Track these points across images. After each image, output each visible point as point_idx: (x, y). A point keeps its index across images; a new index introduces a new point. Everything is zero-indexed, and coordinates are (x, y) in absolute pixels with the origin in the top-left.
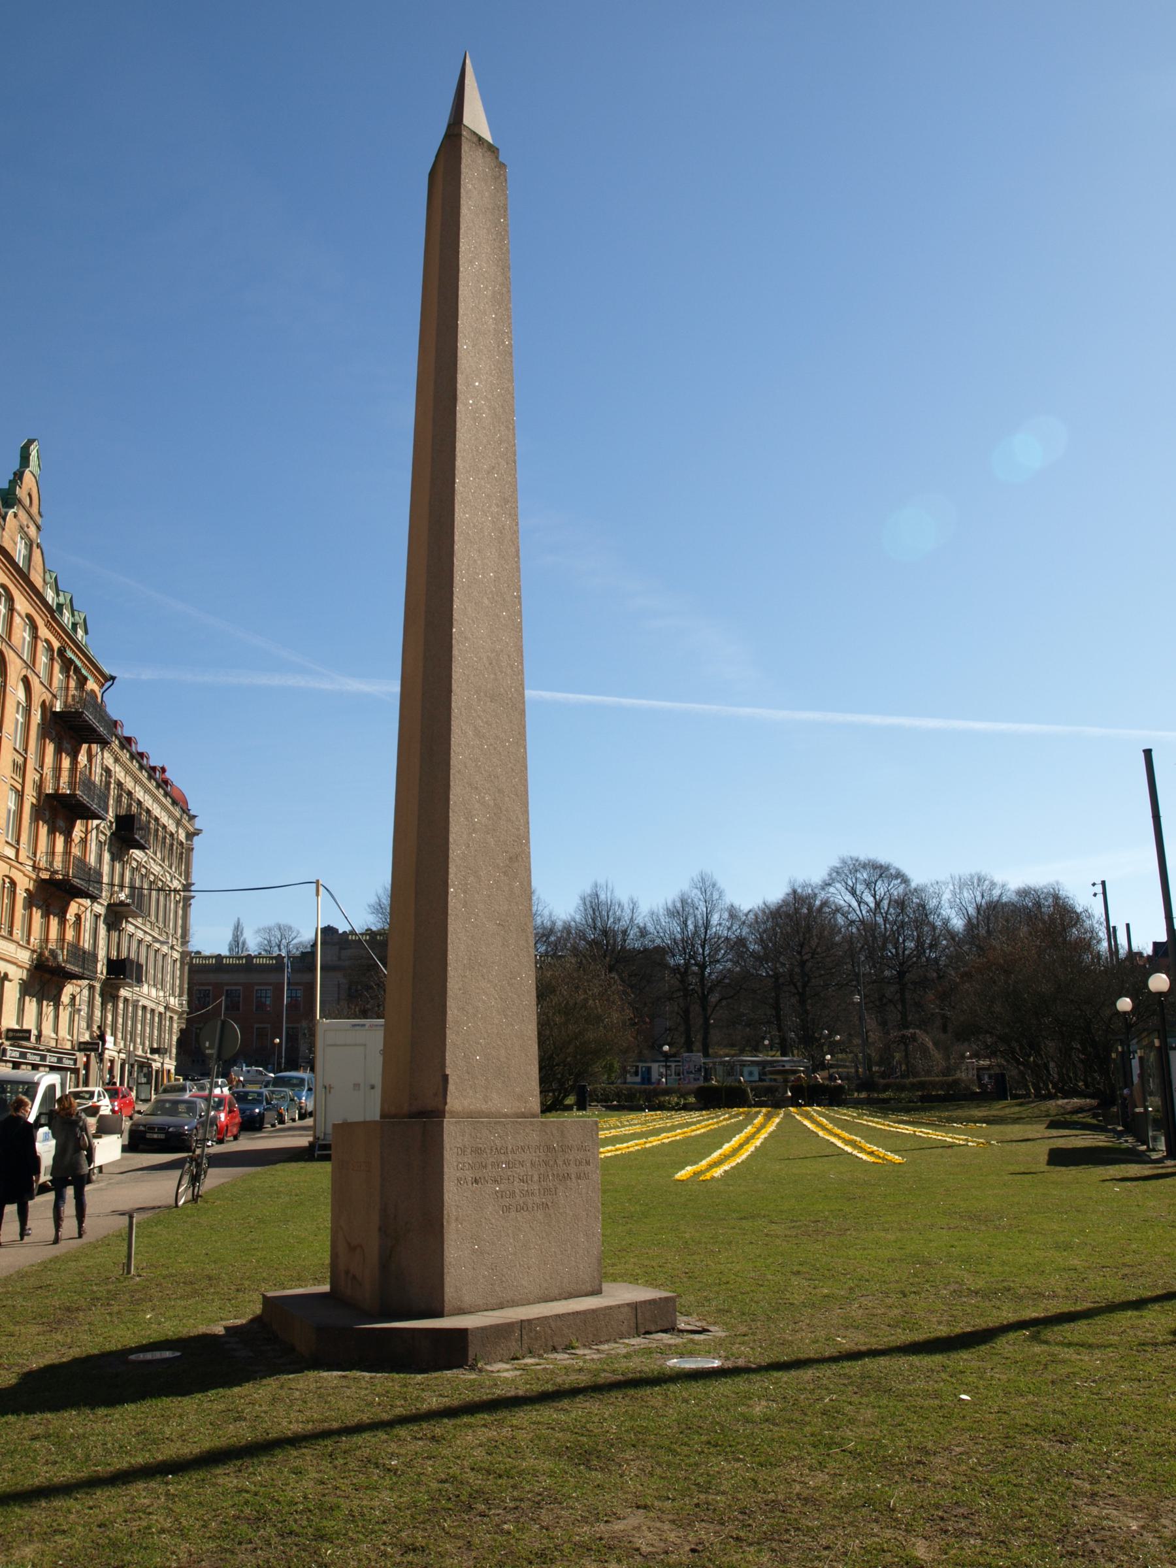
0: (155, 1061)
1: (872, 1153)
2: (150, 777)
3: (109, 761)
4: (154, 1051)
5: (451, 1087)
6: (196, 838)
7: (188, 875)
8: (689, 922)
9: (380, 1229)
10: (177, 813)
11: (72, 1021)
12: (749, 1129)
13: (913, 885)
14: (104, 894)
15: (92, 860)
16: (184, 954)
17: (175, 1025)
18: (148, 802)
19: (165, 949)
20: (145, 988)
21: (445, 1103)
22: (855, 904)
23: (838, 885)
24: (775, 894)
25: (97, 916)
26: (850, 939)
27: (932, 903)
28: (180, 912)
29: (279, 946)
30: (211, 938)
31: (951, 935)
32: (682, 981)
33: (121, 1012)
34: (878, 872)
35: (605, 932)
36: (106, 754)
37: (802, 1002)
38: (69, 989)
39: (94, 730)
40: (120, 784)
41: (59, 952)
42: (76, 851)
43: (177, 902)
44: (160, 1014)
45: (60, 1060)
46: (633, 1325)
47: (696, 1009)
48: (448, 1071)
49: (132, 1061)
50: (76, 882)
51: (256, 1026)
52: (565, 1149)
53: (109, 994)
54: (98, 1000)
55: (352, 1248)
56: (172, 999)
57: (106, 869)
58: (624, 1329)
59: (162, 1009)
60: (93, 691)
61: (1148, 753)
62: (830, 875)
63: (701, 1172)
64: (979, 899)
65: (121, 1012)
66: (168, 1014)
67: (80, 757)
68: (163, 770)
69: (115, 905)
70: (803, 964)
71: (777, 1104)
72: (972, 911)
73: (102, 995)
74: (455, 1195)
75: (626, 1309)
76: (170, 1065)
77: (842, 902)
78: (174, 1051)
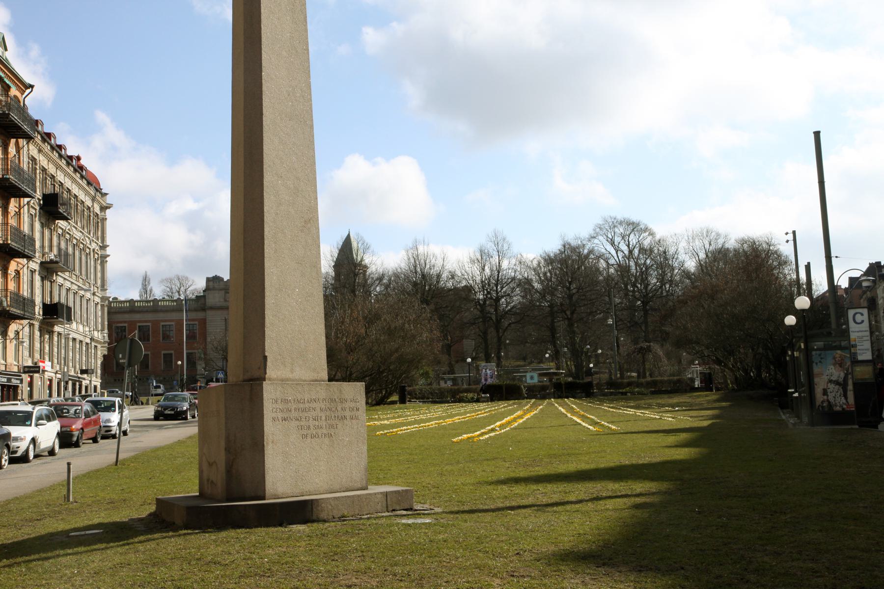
0: (84, 379)
1: (595, 424)
2: (68, 164)
3: (34, 152)
4: (83, 372)
5: (269, 364)
6: (108, 211)
7: (103, 239)
8: (486, 268)
9: (226, 449)
10: (92, 192)
11: (17, 350)
12: (519, 413)
13: (658, 237)
14: (37, 255)
15: (26, 229)
16: (103, 299)
17: (99, 353)
18: (68, 183)
19: (88, 295)
20: (74, 325)
21: (266, 373)
22: (613, 252)
23: (601, 238)
24: (553, 247)
25: (33, 272)
26: (609, 277)
27: (672, 250)
28: (99, 267)
29: (179, 292)
30: (126, 291)
31: (686, 274)
32: (482, 311)
33: (55, 343)
34: (631, 227)
35: (424, 276)
36: (31, 147)
37: (571, 325)
38: (13, 327)
39: (19, 128)
40: (44, 170)
41: (4, 299)
42: (12, 222)
43: (96, 260)
44: (87, 344)
45: (9, 380)
46: (385, 505)
47: (492, 333)
48: (267, 354)
49: (66, 379)
50: (14, 245)
51: (163, 352)
52: (343, 401)
53: (46, 328)
54: (37, 333)
55: (210, 465)
56: (96, 333)
57: (37, 236)
58: (379, 507)
59: (88, 341)
60: (15, 96)
61: (817, 134)
62: (594, 230)
63: (474, 437)
64: (707, 246)
65: (55, 343)
66: (93, 344)
67: (10, 149)
68: (78, 158)
69: (46, 262)
70: (570, 297)
71: (544, 398)
72: (702, 255)
73: (40, 330)
74: (270, 427)
75: (380, 496)
76: (97, 381)
77: (603, 251)
78: (99, 372)
